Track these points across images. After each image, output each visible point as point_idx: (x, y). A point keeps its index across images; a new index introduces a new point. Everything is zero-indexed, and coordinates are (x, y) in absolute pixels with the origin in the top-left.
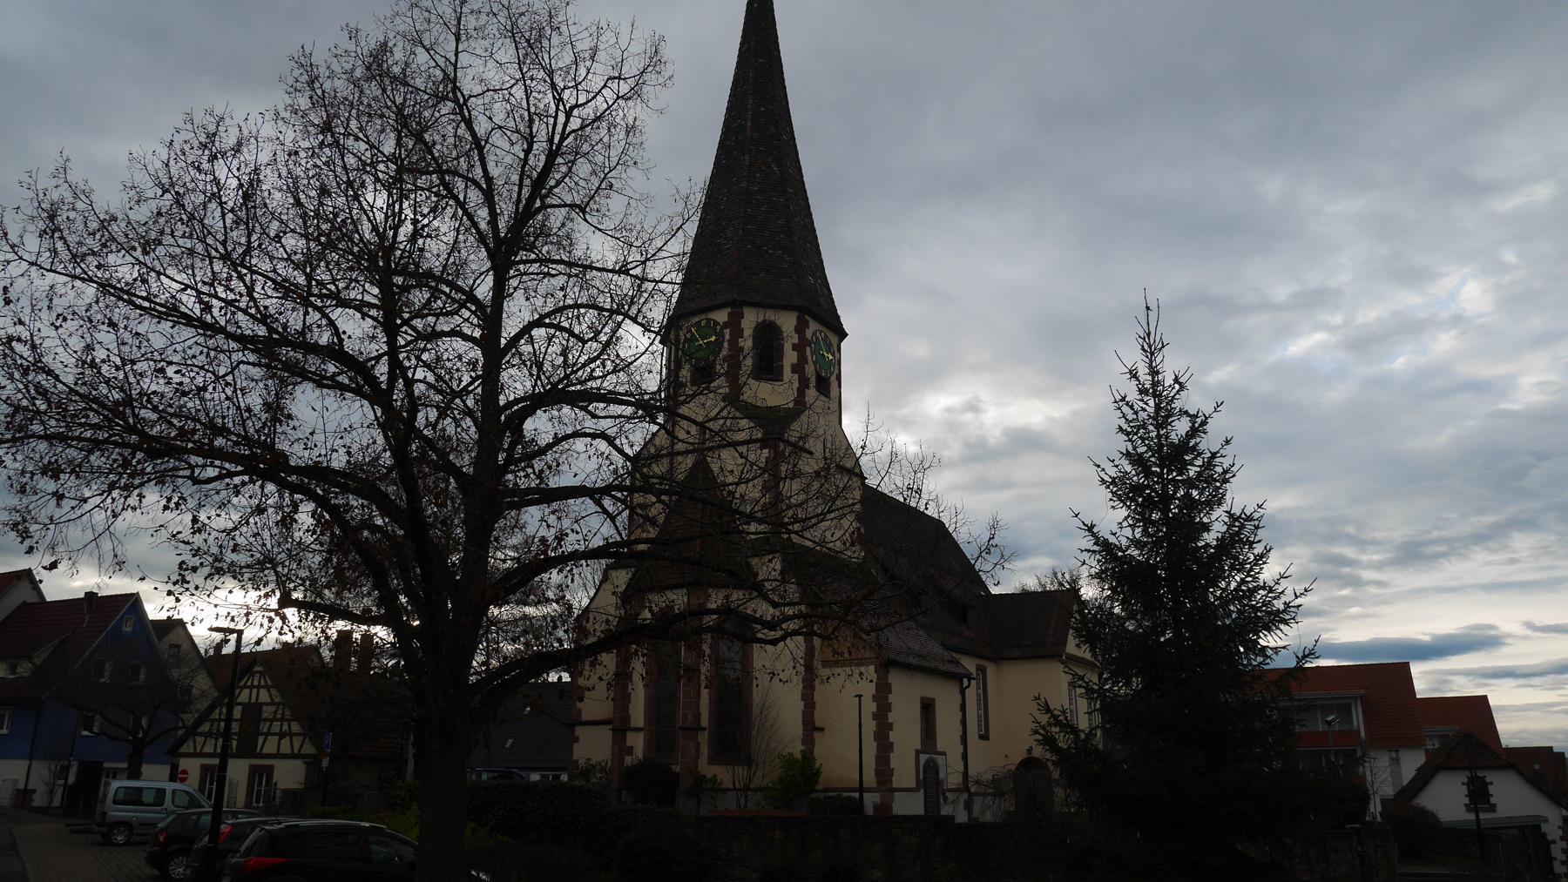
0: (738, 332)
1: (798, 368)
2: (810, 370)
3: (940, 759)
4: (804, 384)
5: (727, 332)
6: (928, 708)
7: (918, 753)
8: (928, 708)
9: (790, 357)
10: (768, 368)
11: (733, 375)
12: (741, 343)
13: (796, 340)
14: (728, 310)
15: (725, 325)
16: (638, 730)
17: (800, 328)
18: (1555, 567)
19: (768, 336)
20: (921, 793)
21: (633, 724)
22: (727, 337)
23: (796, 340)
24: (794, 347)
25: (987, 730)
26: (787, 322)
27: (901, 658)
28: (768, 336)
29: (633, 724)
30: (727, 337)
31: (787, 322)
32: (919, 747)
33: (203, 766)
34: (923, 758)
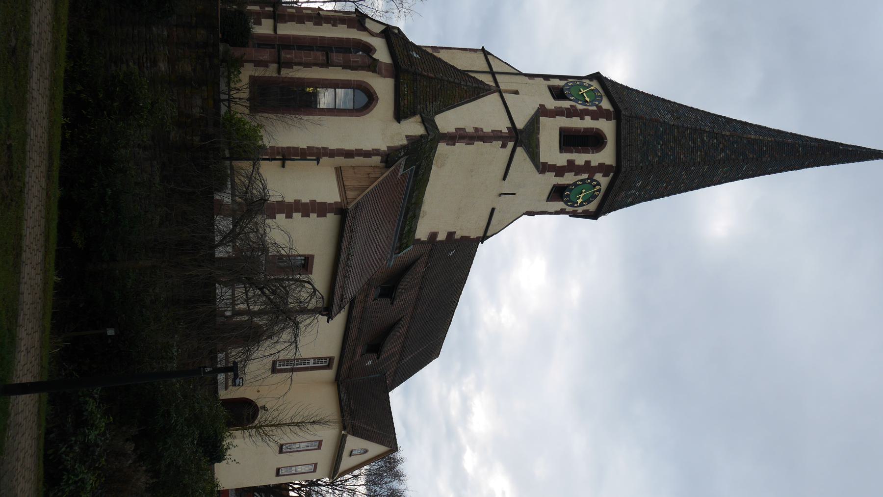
0: (595, 116)
1: (571, 166)
2: (569, 179)
4: (559, 171)
5: (595, 108)
9: (580, 159)
10: (570, 140)
11: (558, 112)
14: (612, 109)
15: (599, 108)
17: (603, 168)
19: (594, 141)
22: (591, 108)
23: (593, 164)
24: (588, 163)
26: (606, 156)
28: (594, 141)
31: (606, 156)
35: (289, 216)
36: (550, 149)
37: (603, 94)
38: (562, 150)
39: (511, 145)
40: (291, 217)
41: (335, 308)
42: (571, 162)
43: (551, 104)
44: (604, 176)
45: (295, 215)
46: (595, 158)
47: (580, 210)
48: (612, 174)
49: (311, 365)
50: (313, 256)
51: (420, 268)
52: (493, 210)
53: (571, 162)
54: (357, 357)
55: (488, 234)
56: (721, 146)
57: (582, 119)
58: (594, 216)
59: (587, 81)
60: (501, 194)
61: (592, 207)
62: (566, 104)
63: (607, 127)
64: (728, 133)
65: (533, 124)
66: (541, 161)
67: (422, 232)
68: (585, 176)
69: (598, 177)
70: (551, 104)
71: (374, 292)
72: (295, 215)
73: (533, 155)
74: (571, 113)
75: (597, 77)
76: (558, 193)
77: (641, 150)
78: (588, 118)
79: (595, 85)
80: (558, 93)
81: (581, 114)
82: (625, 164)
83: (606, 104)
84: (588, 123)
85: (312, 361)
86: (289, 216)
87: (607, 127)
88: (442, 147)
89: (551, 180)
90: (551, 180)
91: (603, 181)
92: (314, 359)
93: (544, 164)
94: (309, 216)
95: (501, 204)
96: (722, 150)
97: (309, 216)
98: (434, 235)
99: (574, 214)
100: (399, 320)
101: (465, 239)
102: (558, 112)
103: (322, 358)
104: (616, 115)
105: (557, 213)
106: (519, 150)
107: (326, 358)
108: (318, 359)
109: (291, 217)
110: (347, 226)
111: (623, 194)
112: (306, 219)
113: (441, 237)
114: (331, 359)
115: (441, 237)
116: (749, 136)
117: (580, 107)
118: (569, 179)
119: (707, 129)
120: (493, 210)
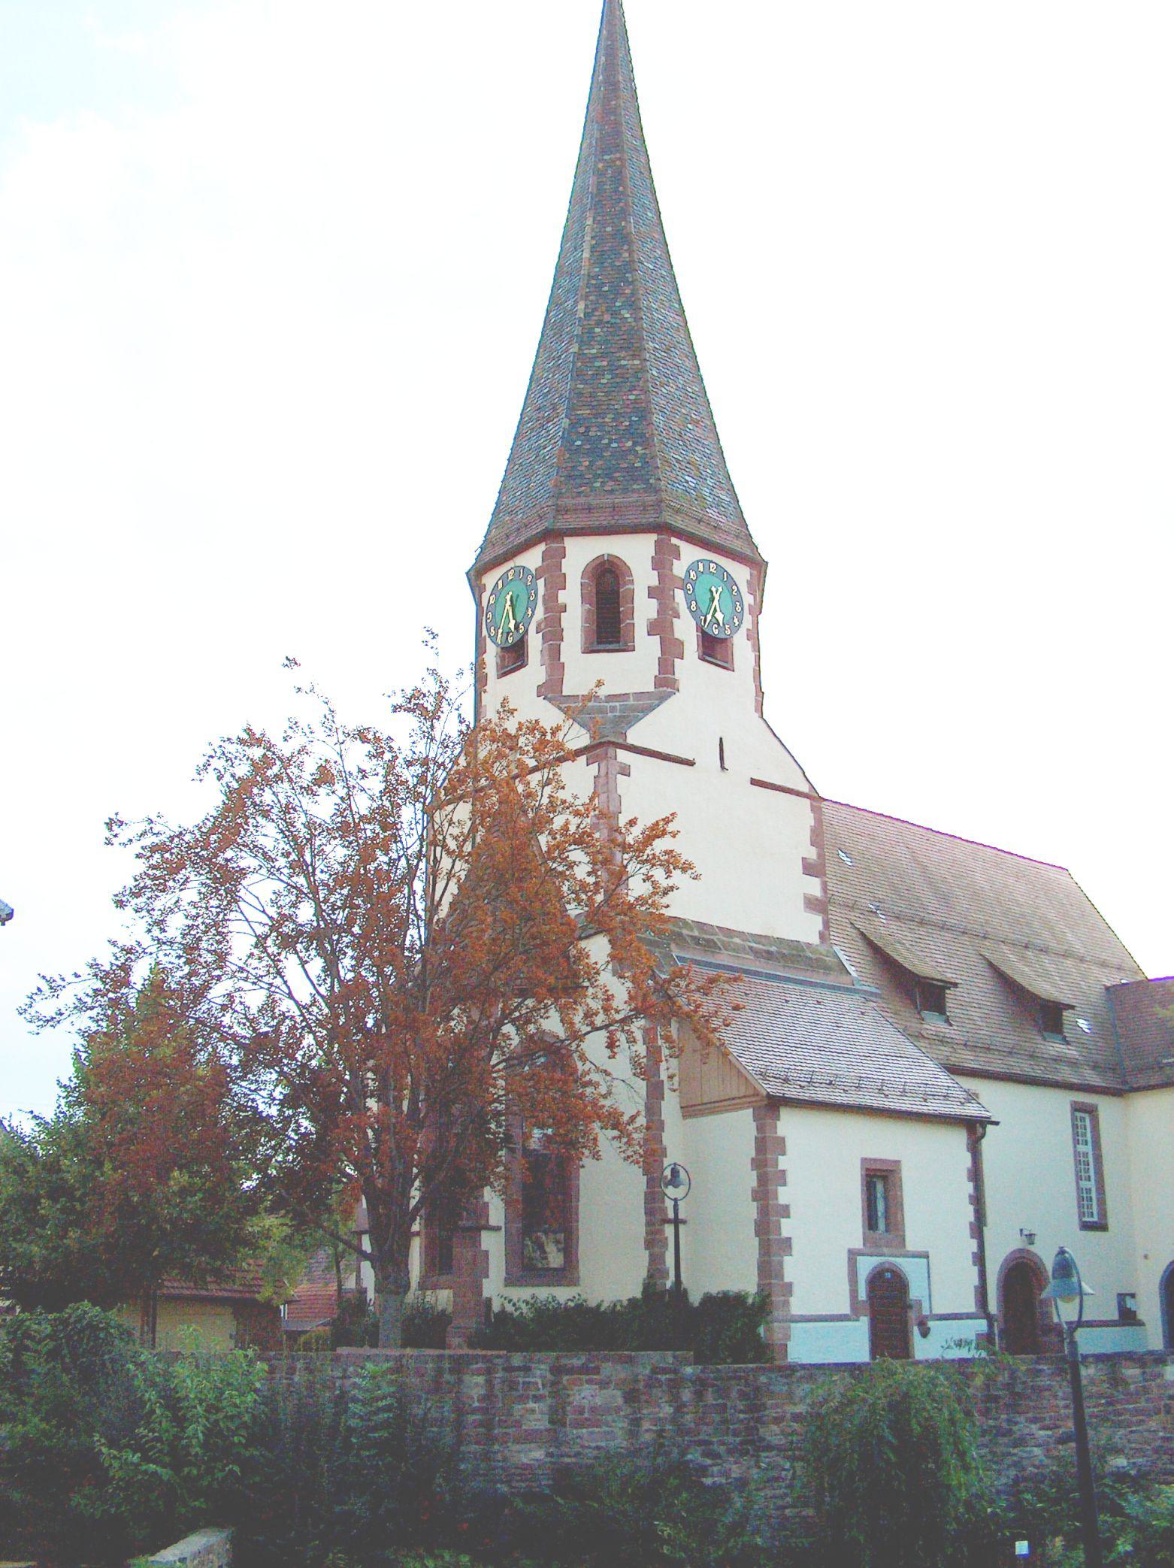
0: (557, 581)
1: (660, 627)
2: (686, 630)
3: (910, 1268)
4: (671, 650)
5: (541, 583)
6: (880, 1182)
7: (853, 1255)
8: (880, 1182)
9: (644, 610)
10: (608, 630)
11: (553, 654)
12: (563, 597)
13: (654, 582)
14: (542, 547)
15: (539, 573)
16: (498, 1229)
17: (662, 561)
18: (590, 509)
19: (607, 586)
20: (864, 1322)
21: (492, 1222)
22: (541, 591)
23: (654, 582)
24: (652, 593)
25: (1103, 1214)
26: (636, 552)
27: (791, 1092)
28: (607, 586)
29: (492, 1222)
30: (541, 591)
31: (636, 552)
32: (858, 1244)
33: (574, 1282)
34: (866, 1265)
35: (785, 1212)
36: (628, 672)
37: (510, 564)
38: (628, 648)
39: (623, 756)
40: (786, 1208)
41: (972, 1110)
42: (654, 628)
43: (535, 671)
44: (678, 558)
45: (782, 1199)
46: (643, 577)
47: (748, 599)
48: (674, 541)
49: (1088, 1149)
50: (864, 1160)
51: (883, 930)
52: (755, 782)
53: (654, 628)
54: (1072, 1052)
55: (804, 788)
56: (607, 317)
57: (564, 609)
58: (758, 566)
59: (485, 597)
60: (723, 767)
61: (741, 573)
62: (535, 643)
63: (580, 554)
64: (581, 306)
65: (577, 709)
66: (652, 689)
67: (806, 929)
68: (679, 595)
69: (679, 568)
70: (535, 671)
71: (933, 1024)
72: (782, 1199)
73: (642, 706)
74: (553, 634)
75: (476, 576)
76: (714, 648)
77: (611, 451)
78: (563, 597)
79: (490, 580)
80: (515, 656)
81: (554, 611)
82: (650, 518)
83: (532, 559)
84: (572, 596)
85: (1081, 1148)
86: (785, 1212)
87: (580, 554)
88: (367, 1227)
89: (690, 667)
90: (690, 667)
91: (690, 554)
92: (1076, 1142)
93: (659, 682)
94: (790, 1284)
95: (742, 767)
96: (615, 313)
97: (790, 1284)
98: (813, 905)
99: (757, 609)
100: (991, 965)
101: (817, 837)
102: (553, 654)
103: (1075, 1126)
104: (553, 535)
105: (757, 648)
106: (634, 737)
107: (1074, 1119)
108: (1075, 1134)
109: (786, 1208)
110: (805, 1095)
111: (712, 513)
112: (789, 1178)
113: (814, 887)
114: (1077, 1108)
115: (814, 887)
116: (585, 264)
117: (540, 613)
118: (686, 630)
119: (575, 348)
120: (755, 782)
